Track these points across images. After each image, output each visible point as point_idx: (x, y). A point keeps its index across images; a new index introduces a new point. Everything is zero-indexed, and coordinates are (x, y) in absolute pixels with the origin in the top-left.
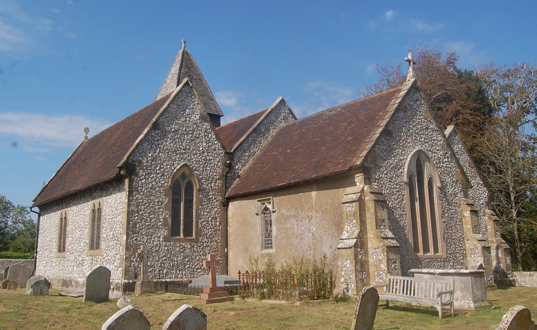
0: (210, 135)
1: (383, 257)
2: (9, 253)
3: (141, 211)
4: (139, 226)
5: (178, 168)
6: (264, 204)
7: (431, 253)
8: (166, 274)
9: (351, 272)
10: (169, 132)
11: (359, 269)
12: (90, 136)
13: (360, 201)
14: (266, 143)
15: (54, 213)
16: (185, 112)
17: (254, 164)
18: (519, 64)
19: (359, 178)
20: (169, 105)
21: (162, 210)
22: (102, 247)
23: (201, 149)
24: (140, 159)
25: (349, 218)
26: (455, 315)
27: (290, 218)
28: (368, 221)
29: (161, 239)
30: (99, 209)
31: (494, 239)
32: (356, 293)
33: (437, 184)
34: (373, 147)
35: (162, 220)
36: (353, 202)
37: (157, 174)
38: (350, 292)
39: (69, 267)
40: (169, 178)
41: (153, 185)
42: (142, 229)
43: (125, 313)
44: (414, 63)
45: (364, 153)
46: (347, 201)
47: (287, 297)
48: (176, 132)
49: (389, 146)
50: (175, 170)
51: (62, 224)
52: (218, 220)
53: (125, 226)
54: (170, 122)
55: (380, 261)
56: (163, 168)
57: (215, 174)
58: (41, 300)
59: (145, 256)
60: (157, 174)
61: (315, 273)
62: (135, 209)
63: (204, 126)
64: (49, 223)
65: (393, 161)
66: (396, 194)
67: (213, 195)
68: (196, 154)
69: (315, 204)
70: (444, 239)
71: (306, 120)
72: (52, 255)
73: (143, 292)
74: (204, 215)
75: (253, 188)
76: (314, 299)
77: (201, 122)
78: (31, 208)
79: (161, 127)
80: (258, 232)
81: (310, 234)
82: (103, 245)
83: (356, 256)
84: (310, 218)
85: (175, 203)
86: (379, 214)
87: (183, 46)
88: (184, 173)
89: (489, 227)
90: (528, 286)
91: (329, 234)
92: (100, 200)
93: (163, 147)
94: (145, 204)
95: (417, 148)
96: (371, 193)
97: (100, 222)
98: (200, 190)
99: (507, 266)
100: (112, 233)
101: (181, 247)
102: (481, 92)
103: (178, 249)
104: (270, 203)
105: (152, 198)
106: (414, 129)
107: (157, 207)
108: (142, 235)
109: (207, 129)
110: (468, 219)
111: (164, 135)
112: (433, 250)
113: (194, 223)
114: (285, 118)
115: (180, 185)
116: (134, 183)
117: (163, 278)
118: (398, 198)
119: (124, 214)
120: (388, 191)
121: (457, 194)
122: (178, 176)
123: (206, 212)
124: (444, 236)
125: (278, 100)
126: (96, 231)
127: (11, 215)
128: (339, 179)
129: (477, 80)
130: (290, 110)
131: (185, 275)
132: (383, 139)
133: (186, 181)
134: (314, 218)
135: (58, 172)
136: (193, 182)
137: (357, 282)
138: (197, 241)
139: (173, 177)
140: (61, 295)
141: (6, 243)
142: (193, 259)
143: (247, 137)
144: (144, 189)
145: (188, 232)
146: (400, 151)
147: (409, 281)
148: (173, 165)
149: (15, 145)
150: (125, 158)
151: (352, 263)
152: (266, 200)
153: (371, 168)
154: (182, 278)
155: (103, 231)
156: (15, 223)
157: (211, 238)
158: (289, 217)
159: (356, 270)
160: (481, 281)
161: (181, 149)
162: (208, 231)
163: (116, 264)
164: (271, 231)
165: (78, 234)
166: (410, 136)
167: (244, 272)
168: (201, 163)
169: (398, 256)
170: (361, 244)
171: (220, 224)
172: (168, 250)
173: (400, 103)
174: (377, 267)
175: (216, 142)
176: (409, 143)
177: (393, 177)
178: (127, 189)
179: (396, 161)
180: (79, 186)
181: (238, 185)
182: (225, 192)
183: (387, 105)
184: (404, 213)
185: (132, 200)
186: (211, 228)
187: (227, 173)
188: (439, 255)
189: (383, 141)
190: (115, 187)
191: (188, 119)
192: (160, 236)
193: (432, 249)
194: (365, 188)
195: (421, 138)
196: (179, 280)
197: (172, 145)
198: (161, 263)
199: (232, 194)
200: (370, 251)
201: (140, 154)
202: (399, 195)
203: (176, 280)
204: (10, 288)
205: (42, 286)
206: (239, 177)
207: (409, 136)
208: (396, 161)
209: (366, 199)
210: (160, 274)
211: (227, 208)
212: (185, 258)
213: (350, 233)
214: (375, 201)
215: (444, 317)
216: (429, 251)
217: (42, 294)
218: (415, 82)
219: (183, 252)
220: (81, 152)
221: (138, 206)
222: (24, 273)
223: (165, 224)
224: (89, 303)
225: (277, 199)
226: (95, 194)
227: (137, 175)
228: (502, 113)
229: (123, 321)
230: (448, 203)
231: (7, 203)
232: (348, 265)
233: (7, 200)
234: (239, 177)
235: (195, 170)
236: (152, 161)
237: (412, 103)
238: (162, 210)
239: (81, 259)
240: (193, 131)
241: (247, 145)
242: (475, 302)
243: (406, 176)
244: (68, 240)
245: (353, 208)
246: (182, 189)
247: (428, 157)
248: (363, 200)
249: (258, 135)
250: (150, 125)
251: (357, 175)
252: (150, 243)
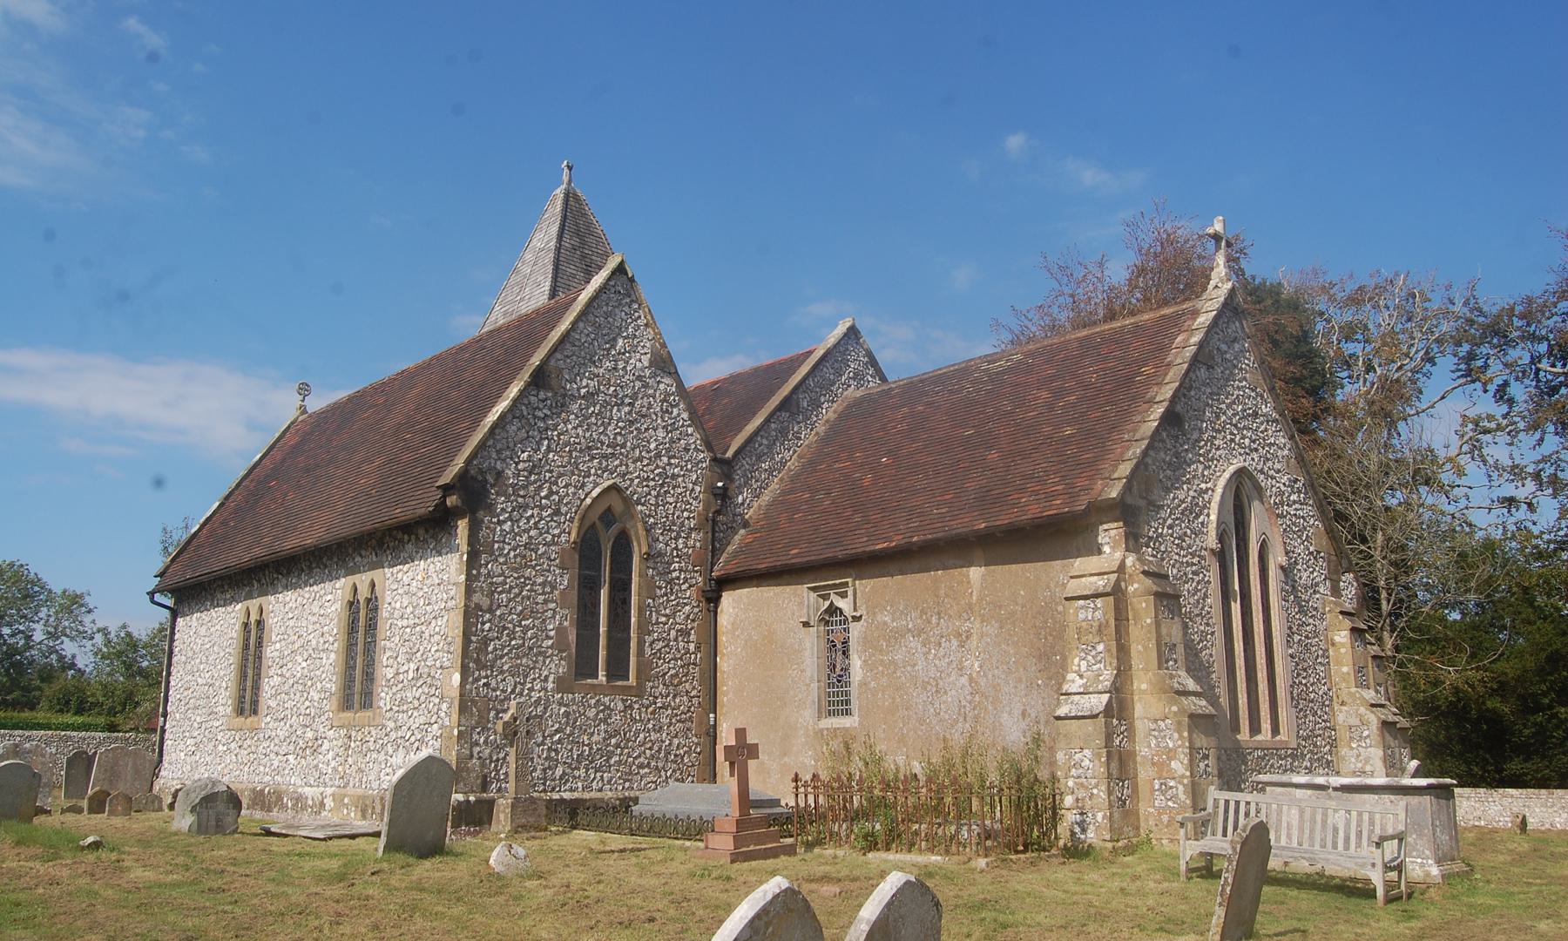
0: (675, 411)
1: (1175, 740)
2: (40, 716)
3: (499, 606)
4: (495, 649)
5: (595, 494)
9: (1094, 781)
10: (573, 398)
11: (1115, 773)
13: (1117, 593)
14: (813, 438)
15: (221, 609)
16: (613, 346)
17: (783, 493)
18: (1386, 273)
19: (1110, 535)
20: (574, 323)
22: (382, 704)
23: (653, 446)
24: (499, 465)
25: (1084, 639)
27: (903, 636)
28: (1136, 649)
30: (368, 601)
32: (1108, 837)
33: (1277, 558)
34: (1145, 453)
37: (542, 508)
38: (1091, 834)
39: (273, 756)
40: (572, 520)
42: (502, 657)
43: (771, 902)
44: (1229, 245)
45: (1125, 469)
46: (1079, 593)
47: (949, 845)
48: (590, 396)
49: (1177, 455)
50: (588, 501)
51: (246, 640)
52: (692, 637)
53: (457, 647)
55: (1171, 754)
56: (557, 493)
58: (223, 849)
59: (523, 730)
61: (1018, 781)
62: (485, 602)
63: (662, 386)
64: (208, 636)
68: (640, 459)
69: (980, 599)
71: (921, 381)
72: (217, 724)
73: (517, 830)
74: (657, 623)
75: (795, 555)
76: (1017, 852)
77: (654, 376)
78: (152, 594)
79: (553, 382)
80: (809, 673)
81: (964, 680)
82: (384, 698)
83: (1109, 738)
84: (963, 638)
85: (588, 587)
86: (1164, 631)
87: (565, 179)
91: (1020, 680)
92: (376, 575)
95: (1237, 464)
96: (1145, 573)
97: (374, 636)
98: (648, 557)
100: (413, 666)
101: (599, 706)
102: (1304, 337)
103: (591, 713)
104: (843, 595)
106: (1230, 413)
107: (541, 599)
108: (502, 672)
109: (668, 395)
110: (1343, 650)
113: (633, 644)
114: (858, 376)
115: (598, 541)
118: (1196, 590)
119: (452, 614)
121: (1317, 585)
122: (594, 516)
123: (662, 612)
125: (841, 329)
126: (359, 660)
127: (41, 615)
128: (1058, 535)
129: (1294, 306)
130: (869, 354)
131: (609, 782)
133: (614, 530)
134: (975, 637)
135: (227, 498)
136: (632, 533)
137: (1111, 806)
138: (639, 691)
139: (582, 519)
140: (268, 833)
141: (27, 690)
142: (628, 740)
143: (767, 421)
145: (617, 668)
146: (1201, 467)
147: (1232, 804)
148: (583, 485)
150: (459, 463)
151: (1099, 756)
152: (835, 586)
153: (1139, 508)
154: (600, 790)
155: (384, 658)
156: (53, 636)
157: (674, 685)
158: (900, 634)
159: (1110, 775)
162: (668, 667)
164: (846, 669)
165: (300, 666)
167: (808, 777)
169: (1213, 741)
170: (1118, 709)
171: (698, 648)
172: (567, 714)
173: (1201, 345)
174: (1161, 767)
175: (690, 430)
178: (464, 548)
180: (311, 534)
181: (743, 550)
182: (713, 565)
183: (1163, 349)
186: (676, 659)
187: (718, 512)
189: (1163, 441)
190: (425, 540)
191: (621, 365)
193: (1266, 725)
194: (1130, 561)
195: (1243, 438)
196: (594, 795)
197: (580, 431)
198: (550, 749)
199: (732, 569)
200: (1141, 726)
201: (499, 452)
203: (586, 796)
204: (111, 813)
205: (221, 806)
206: (746, 524)
207: (1218, 431)
210: (545, 779)
212: (611, 737)
213: (1086, 679)
214: (1156, 594)
215: (1390, 900)
217: (220, 828)
218: (1232, 292)
219: (605, 721)
220: (294, 447)
222: (137, 771)
223: (561, 645)
224: (400, 858)
225: (865, 586)
226: (358, 559)
227: (490, 509)
228: (1350, 392)
229: (767, 925)
230: (1301, 606)
231: (32, 582)
232: (1086, 763)
233: (32, 575)
234: (746, 524)
235: (638, 502)
236: (530, 473)
237: (1224, 347)
239: (310, 735)
240: (634, 397)
244: (269, 685)
245: (1100, 611)
246: (604, 553)
247: (1259, 489)
249: (792, 415)
250: (525, 375)
251: (1106, 526)
252: (521, 694)
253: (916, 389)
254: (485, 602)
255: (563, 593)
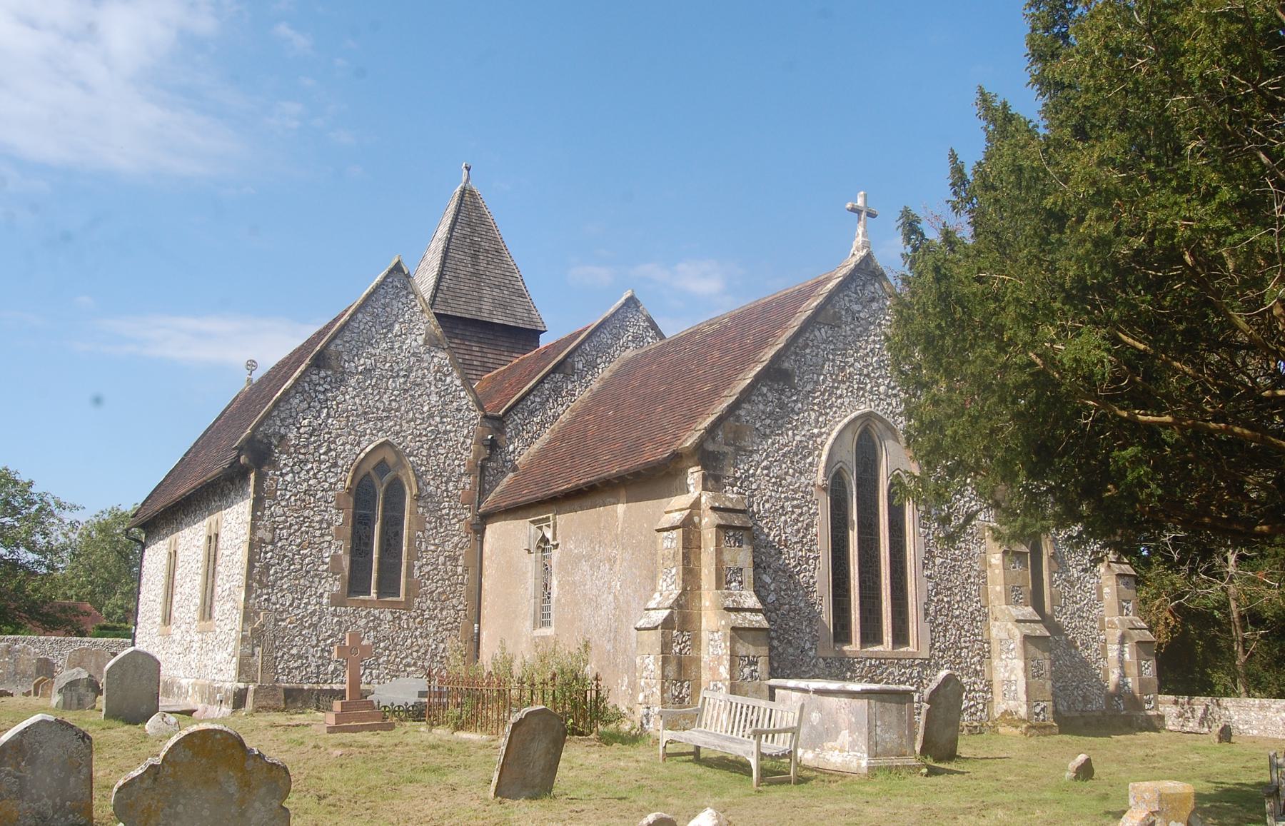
0: (449, 379)
5: (368, 450)
6: (540, 528)
7: (887, 645)
8: (333, 673)
10: (351, 374)
12: (256, 376)
13: (689, 527)
14: (587, 394)
16: (390, 331)
19: (694, 476)
21: (329, 538)
23: (426, 409)
26: (801, 780)
29: (325, 601)
31: (1116, 620)
35: (327, 560)
36: (673, 528)
37: (320, 462)
41: (310, 486)
42: (282, 578)
48: (367, 372)
49: (782, 406)
50: (362, 455)
52: (461, 562)
54: (354, 352)
57: (457, 462)
60: (320, 462)
62: (268, 536)
63: (436, 360)
65: (788, 439)
66: (793, 512)
67: (450, 508)
68: (414, 420)
70: (926, 614)
74: (427, 551)
75: (525, 496)
79: (334, 363)
81: (611, 597)
83: (666, 646)
84: (612, 561)
85: (361, 524)
86: (727, 556)
87: (464, 178)
88: (383, 461)
89: (1106, 590)
90: (1255, 732)
93: (338, 404)
94: (291, 525)
95: (863, 409)
96: (714, 509)
98: (418, 497)
99: (1143, 685)
101: (371, 618)
103: (362, 622)
105: (306, 514)
107: (318, 533)
108: (282, 590)
111: (340, 380)
112: (890, 639)
115: (373, 487)
116: (268, 483)
117: (326, 681)
120: (767, 506)
123: (430, 545)
124: (926, 610)
128: (652, 479)
130: (649, 320)
131: (378, 677)
132: (765, 390)
133: (387, 478)
138: (408, 606)
143: (541, 381)
144: (289, 494)
145: (388, 585)
146: (813, 415)
148: (359, 443)
149: (98, 401)
153: (725, 454)
157: (441, 600)
159: (664, 676)
160: (899, 712)
161: (378, 409)
163: (230, 650)
166: (844, 383)
168: (424, 439)
170: (681, 620)
171: (466, 571)
172: (339, 623)
174: (714, 670)
175: (462, 394)
176: (841, 396)
177: (787, 473)
179: (798, 438)
184: (812, 555)
185: (261, 518)
186: (444, 580)
187: (488, 459)
188: (907, 652)
191: (397, 345)
192: (322, 595)
194: (703, 500)
197: (357, 400)
200: (705, 636)
202: (801, 514)
206: (515, 469)
208: (798, 438)
209: (703, 522)
210: (318, 673)
211: (482, 537)
212: (380, 641)
216: (879, 641)
219: (375, 628)
221: (275, 529)
223: (335, 568)
224: (112, 723)
225: (562, 519)
227: (274, 465)
238: (329, 538)
240: (410, 370)
241: (538, 400)
242: (874, 754)
243: (821, 471)
245: (672, 542)
248: (697, 526)
249: (567, 377)
251: (691, 470)
252: (298, 607)
253: (679, 341)
254: (268, 537)
255: (338, 528)
